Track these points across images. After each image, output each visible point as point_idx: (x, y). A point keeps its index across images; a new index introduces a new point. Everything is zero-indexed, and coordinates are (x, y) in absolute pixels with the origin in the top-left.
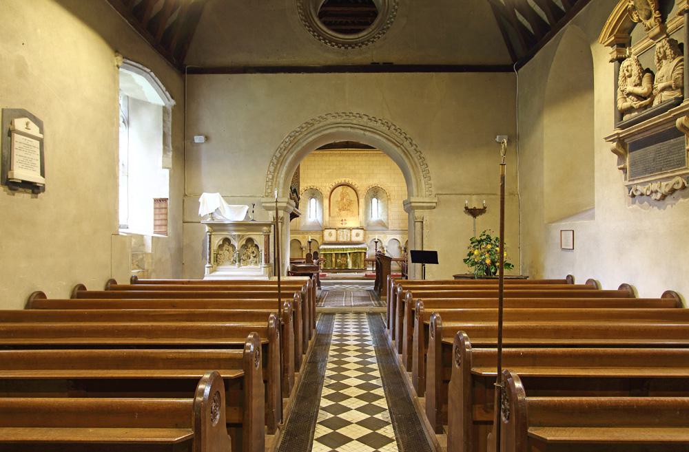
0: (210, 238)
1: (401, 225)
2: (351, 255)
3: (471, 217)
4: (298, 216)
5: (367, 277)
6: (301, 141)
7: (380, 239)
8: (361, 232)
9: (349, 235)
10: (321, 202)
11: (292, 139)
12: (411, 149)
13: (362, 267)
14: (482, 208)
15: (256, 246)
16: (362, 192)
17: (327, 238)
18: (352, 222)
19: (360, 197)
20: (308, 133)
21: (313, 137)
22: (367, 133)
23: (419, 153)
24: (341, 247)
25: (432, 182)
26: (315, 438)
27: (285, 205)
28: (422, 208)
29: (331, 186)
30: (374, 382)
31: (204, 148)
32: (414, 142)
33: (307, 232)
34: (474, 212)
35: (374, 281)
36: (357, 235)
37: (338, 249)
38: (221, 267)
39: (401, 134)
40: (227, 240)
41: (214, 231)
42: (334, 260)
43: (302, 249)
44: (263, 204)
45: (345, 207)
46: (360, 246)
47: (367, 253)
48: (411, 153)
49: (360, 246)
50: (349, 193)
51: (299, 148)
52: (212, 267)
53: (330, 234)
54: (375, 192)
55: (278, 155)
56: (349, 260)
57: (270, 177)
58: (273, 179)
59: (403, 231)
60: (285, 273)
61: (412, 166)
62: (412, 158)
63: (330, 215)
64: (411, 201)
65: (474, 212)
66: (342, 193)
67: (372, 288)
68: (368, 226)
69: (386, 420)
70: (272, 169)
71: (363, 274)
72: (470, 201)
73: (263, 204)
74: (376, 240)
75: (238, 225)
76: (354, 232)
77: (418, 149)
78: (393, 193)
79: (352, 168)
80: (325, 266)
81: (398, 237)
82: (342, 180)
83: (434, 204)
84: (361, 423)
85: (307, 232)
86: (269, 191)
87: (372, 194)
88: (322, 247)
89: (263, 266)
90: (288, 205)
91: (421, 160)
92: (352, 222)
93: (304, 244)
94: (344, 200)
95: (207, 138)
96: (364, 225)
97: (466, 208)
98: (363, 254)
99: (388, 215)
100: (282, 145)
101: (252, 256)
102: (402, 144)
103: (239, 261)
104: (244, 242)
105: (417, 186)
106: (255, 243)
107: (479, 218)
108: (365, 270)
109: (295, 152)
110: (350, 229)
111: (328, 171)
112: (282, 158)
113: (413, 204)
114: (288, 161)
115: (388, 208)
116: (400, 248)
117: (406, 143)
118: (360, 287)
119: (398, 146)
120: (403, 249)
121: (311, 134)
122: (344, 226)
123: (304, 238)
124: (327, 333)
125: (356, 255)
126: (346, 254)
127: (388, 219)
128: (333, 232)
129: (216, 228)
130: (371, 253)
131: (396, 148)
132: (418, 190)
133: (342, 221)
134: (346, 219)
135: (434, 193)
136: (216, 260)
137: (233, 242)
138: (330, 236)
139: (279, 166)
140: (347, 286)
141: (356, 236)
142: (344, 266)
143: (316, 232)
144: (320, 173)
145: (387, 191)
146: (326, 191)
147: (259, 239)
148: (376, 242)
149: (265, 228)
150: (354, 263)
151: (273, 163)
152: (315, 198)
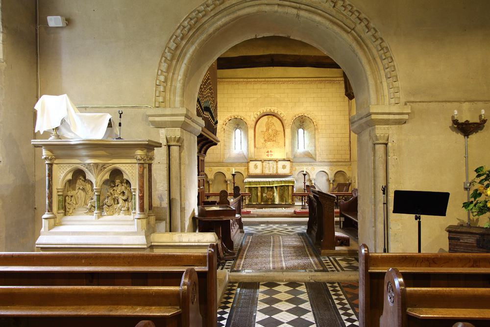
0: (50, 170)
1: (330, 156)
2: (278, 189)
3: (460, 137)
4: (216, 144)
5: (297, 215)
6: (206, 25)
7: (308, 171)
8: (288, 164)
9: (275, 167)
10: (246, 132)
11: (193, 22)
12: (367, 36)
13: (290, 201)
14: (478, 121)
15: (128, 182)
16: (288, 121)
17: (253, 171)
18: (278, 153)
19: (286, 127)
20: (214, 16)
21: (224, 20)
22: (302, 13)
23: (379, 41)
24: (267, 180)
25: (399, 84)
26: (256, 321)
27: (182, 119)
28: (386, 122)
29: (256, 116)
30: (301, 296)
31: (65, 34)
32: (372, 25)
33: (232, 164)
34: (465, 129)
35: (307, 219)
36: (284, 167)
38: (68, 218)
39: (353, 13)
40: (79, 174)
41: (57, 158)
42: (259, 194)
43: (226, 182)
44: (151, 119)
45: (271, 138)
46: (287, 179)
47: (295, 187)
48: (368, 42)
49: (287, 179)
50: (275, 124)
51: (203, 37)
52: (54, 218)
53: (256, 167)
54: (302, 122)
55: (173, 45)
56: (275, 194)
57: (162, 78)
58: (166, 81)
59: (332, 163)
60: (188, 222)
61: (369, 61)
62: (367, 46)
63: (255, 147)
64: (371, 111)
65: (465, 129)
66: (267, 124)
67: (303, 229)
68: (295, 157)
69: (305, 299)
70: (164, 66)
71: (291, 210)
72: (460, 111)
73: (151, 119)
74: (305, 173)
75: (93, 146)
76: (281, 164)
77: (379, 34)
78: (320, 123)
80: (250, 201)
82: (266, 109)
83: (406, 117)
84: (289, 311)
85: (232, 164)
86: (161, 99)
87: (298, 124)
88: (246, 180)
89: (137, 216)
90: (189, 121)
91: (382, 52)
92: (278, 153)
93: (229, 177)
94: (270, 130)
95: (69, 22)
96: (291, 157)
97: (455, 122)
98: (290, 188)
99: (315, 146)
100: (179, 31)
101: (121, 198)
102: (353, 29)
103: (101, 208)
104: (107, 176)
105: (377, 91)
106: (125, 177)
107: (474, 137)
108: (292, 205)
109: (198, 41)
110: (276, 161)
111: (252, 100)
112: (178, 52)
113: (373, 117)
114: (188, 56)
115: (315, 138)
116: (328, 180)
117: (360, 27)
118: (290, 228)
119: (348, 33)
120: (331, 182)
121: (220, 16)
122: (270, 157)
123: (229, 170)
125: (283, 189)
126: (272, 188)
128: (259, 163)
129: (58, 152)
130: (299, 185)
131: (345, 35)
132: (377, 99)
133: (268, 152)
135: (403, 100)
136: (65, 208)
137: (90, 176)
138: (255, 168)
139: (174, 62)
140: (275, 227)
141: (283, 169)
142: (270, 201)
143: (241, 164)
144: (242, 100)
145: (314, 121)
146: (250, 119)
147: (131, 170)
148: (305, 175)
149: (139, 152)
150: (282, 198)
151: (166, 58)
152: (240, 128)
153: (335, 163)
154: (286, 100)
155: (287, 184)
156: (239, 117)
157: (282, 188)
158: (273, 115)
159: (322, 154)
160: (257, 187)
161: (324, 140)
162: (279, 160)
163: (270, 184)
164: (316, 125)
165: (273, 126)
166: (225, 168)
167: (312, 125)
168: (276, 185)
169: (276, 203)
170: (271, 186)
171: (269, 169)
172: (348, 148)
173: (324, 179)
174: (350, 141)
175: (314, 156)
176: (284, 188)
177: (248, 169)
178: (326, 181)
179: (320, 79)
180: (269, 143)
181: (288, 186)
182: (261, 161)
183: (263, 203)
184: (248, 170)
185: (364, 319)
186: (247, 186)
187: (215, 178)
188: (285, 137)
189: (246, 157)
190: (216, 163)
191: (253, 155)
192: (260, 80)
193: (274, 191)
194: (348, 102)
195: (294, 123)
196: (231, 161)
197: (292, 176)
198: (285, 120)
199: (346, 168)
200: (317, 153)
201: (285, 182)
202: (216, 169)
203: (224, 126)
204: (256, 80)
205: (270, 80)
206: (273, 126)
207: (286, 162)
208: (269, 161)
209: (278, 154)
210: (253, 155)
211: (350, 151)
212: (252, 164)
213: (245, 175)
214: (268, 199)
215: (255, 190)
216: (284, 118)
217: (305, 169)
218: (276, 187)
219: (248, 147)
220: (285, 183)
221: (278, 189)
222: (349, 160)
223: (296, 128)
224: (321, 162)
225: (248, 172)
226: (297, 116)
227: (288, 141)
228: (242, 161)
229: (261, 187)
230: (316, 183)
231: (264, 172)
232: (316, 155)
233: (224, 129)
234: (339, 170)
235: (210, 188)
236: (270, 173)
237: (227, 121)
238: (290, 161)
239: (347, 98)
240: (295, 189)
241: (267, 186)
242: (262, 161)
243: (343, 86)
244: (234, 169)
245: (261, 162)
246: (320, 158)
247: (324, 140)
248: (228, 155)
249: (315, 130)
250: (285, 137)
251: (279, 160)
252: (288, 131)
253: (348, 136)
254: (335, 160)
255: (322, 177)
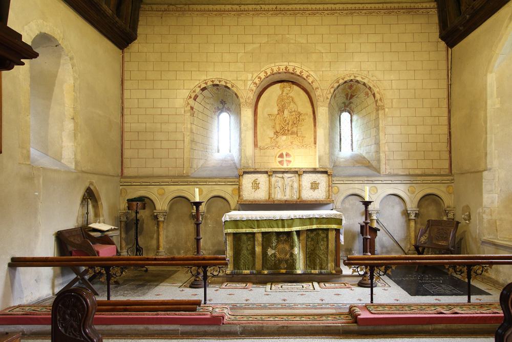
1: (409, 164)
2: (303, 237)
8: (322, 179)
9: (296, 185)
17: (249, 194)
29: (257, 81)
36: (314, 186)
37: (270, 222)
42: (258, 249)
43: (156, 217)
45: (288, 127)
47: (342, 231)
50: (296, 99)
53: (256, 185)
54: (349, 96)
56: (296, 251)
59: (413, 178)
63: (256, 145)
66: (281, 99)
76: (307, 179)
79: (303, 40)
81: (401, 190)
82: (279, 66)
87: (341, 99)
94: (286, 112)
96: (328, 166)
98: (332, 235)
99: (378, 144)
110: (298, 173)
111: (249, 48)
115: (377, 127)
116: (406, 213)
120: (413, 217)
122: (285, 166)
124: (260, 226)
126: (289, 234)
127: (378, 152)
128: (262, 178)
133: (281, 156)
134: (290, 153)
138: (255, 188)
141: (311, 189)
145: (376, 90)
146: (246, 88)
150: (311, 258)
152: (228, 110)
153: (419, 178)
154: (319, 48)
155: (324, 226)
156: (223, 83)
157: (312, 235)
158: (290, 80)
159: (393, 159)
160: (254, 234)
161: (395, 130)
162: (304, 172)
163: (283, 227)
164: (381, 99)
165: (292, 105)
166: (155, 189)
167: (371, 100)
168: (298, 228)
169: (299, 272)
170: (286, 230)
171: (284, 190)
172: (444, 147)
173: (397, 210)
174: (450, 133)
175: (374, 163)
176: (318, 234)
177: (239, 190)
178: (400, 215)
179: (389, 5)
180: (284, 137)
181: (327, 230)
182: (266, 172)
183: (266, 272)
184: (239, 192)
185: (314, 202)
186: (230, 231)
187: (171, 208)
188: (315, 125)
189: (238, 166)
190: (174, 177)
191: (250, 162)
192: (266, 7)
193: (293, 242)
194: (445, 53)
195: (334, 96)
196: (204, 174)
197: (331, 206)
198: (317, 88)
199: (443, 187)
200: (382, 155)
201: (319, 220)
202: (173, 191)
203: (191, 102)
204: (258, 7)
205: (286, 7)
206: (292, 105)
207: (319, 175)
208: (283, 172)
209: (302, 159)
210: (250, 162)
211: (450, 152)
212: (247, 180)
213: (233, 202)
214: (280, 261)
215: (248, 239)
216: (315, 85)
217: (356, 188)
218: (298, 232)
219: (240, 144)
220: (320, 223)
221: (303, 237)
222: (447, 171)
223: (337, 109)
224: (390, 175)
225: (239, 196)
226: (341, 81)
227: (321, 132)
228: (227, 173)
229: (263, 234)
230: (381, 220)
231: (273, 196)
232: (379, 161)
233: (192, 108)
234: (429, 191)
235: (161, 229)
236: (285, 198)
237: (198, 90)
238: (326, 172)
239: (443, 44)
240: (342, 238)
241: (276, 230)
242: (270, 173)
243: (435, 19)
244: (197, 190)
245: (265, 175)
246: (388, 167)
247: (395, 130)
248: (202, 162)
249: (377, 110)
250: (315, 125)
251: (304, 172)
252: (323, 112)
253: (446, 122)
254: (418, 172)
255: (393, 207)
